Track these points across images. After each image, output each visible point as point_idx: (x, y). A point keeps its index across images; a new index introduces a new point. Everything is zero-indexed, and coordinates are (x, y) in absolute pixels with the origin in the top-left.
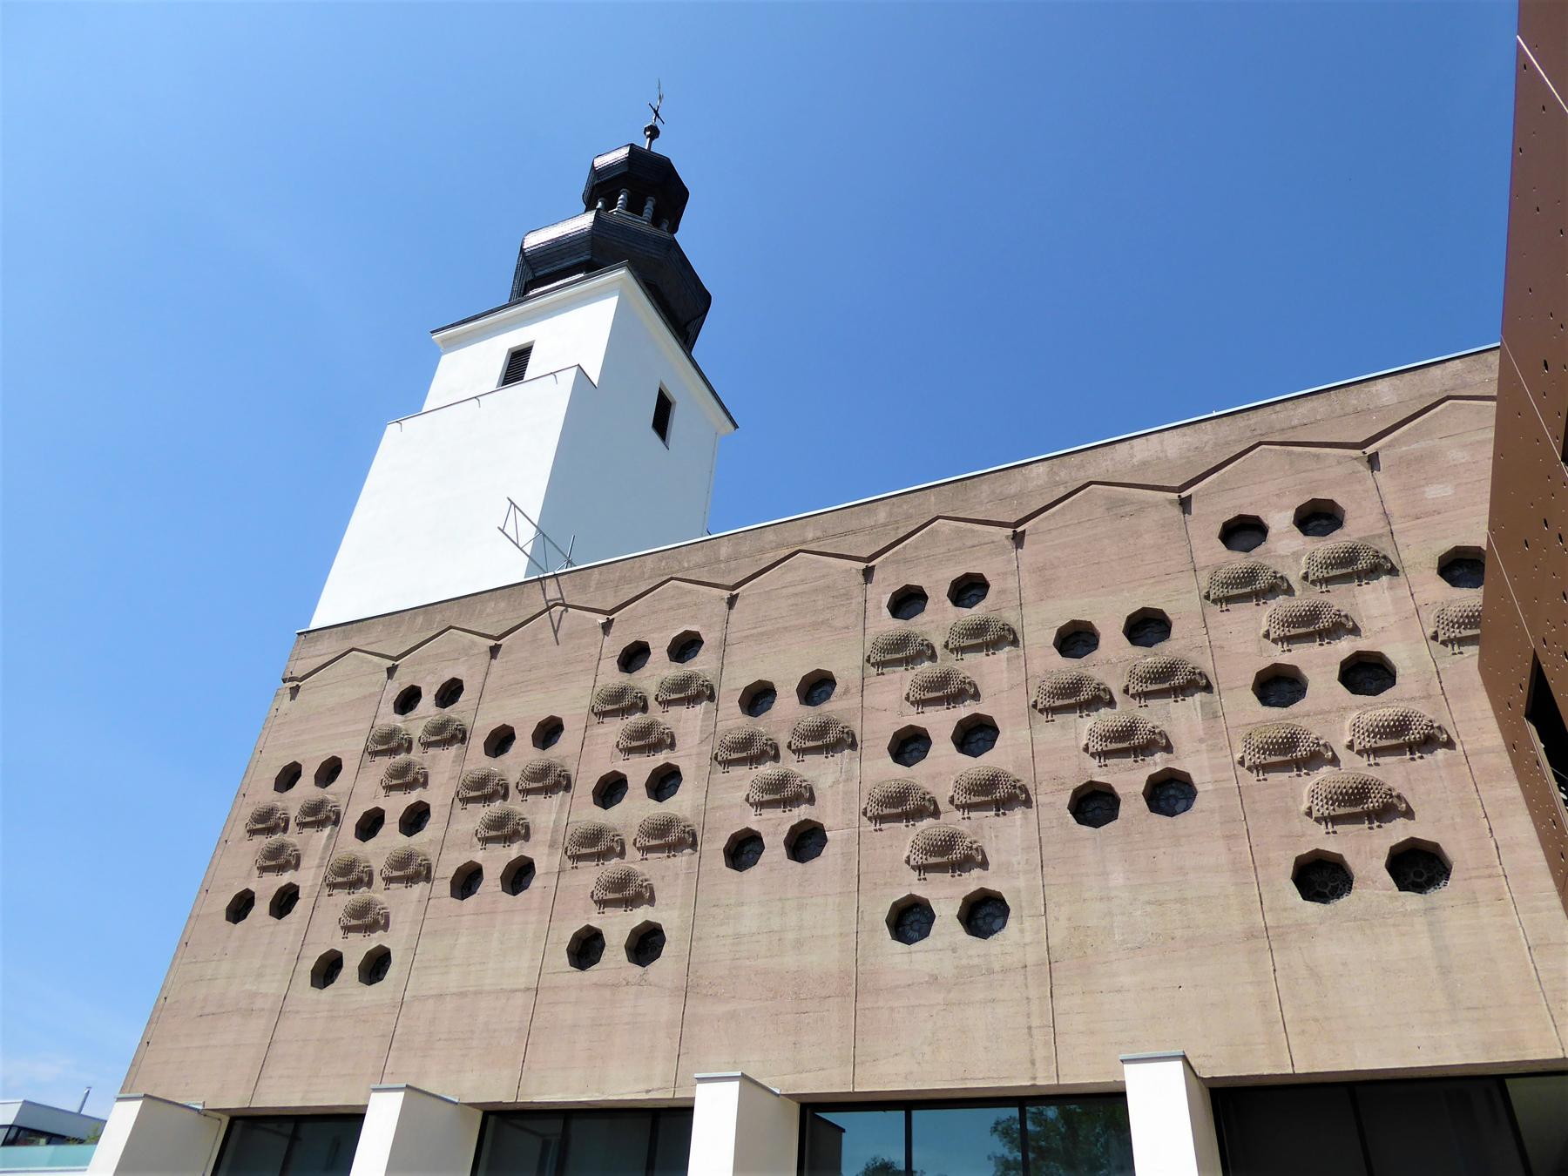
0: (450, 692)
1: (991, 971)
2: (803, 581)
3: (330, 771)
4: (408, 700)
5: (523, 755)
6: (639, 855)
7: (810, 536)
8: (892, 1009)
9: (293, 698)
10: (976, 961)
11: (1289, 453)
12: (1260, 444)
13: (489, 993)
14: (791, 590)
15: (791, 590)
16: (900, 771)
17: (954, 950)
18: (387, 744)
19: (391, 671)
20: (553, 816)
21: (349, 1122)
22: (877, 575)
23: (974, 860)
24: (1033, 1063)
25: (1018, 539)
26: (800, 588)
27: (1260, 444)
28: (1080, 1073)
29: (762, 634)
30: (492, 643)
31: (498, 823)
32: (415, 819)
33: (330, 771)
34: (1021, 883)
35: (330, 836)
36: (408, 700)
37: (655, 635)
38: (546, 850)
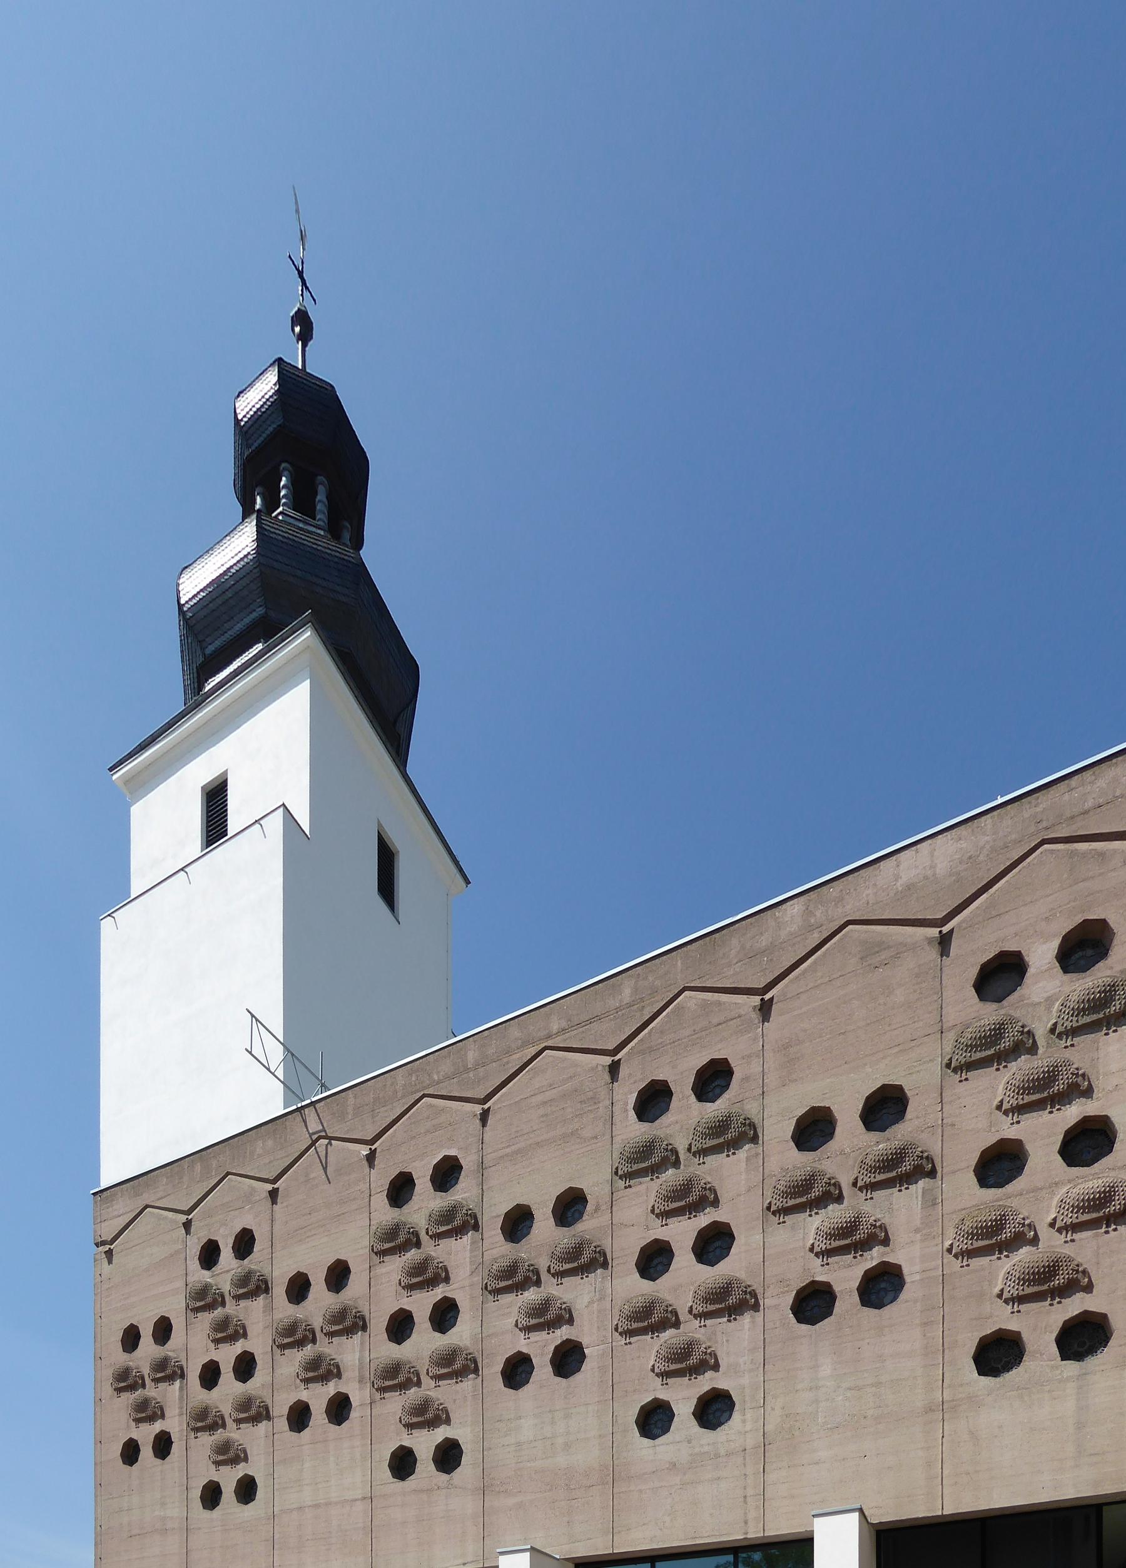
1: (717, 1456)
2: (551, 1086)
6: (432, 1383)
7: (555, 1027)
8: (641, 1491)
10: (706, 1449)
11: (1073, 854)
13: (336, 1503)
14: (540, 1098)
15: (540, 1098)
17: (689, 1442)
20: (357, 1355)
22: (623, 1071)
23: (440, 1418)
24: (746, 1522)
25: (187, 1225)
26: (549, 1095)
28: (780, 1527)
29: (517, 1152)
32: (245, 1367)
34: (746, 1380)
37: (416, 1164)
38: (357, 1385)
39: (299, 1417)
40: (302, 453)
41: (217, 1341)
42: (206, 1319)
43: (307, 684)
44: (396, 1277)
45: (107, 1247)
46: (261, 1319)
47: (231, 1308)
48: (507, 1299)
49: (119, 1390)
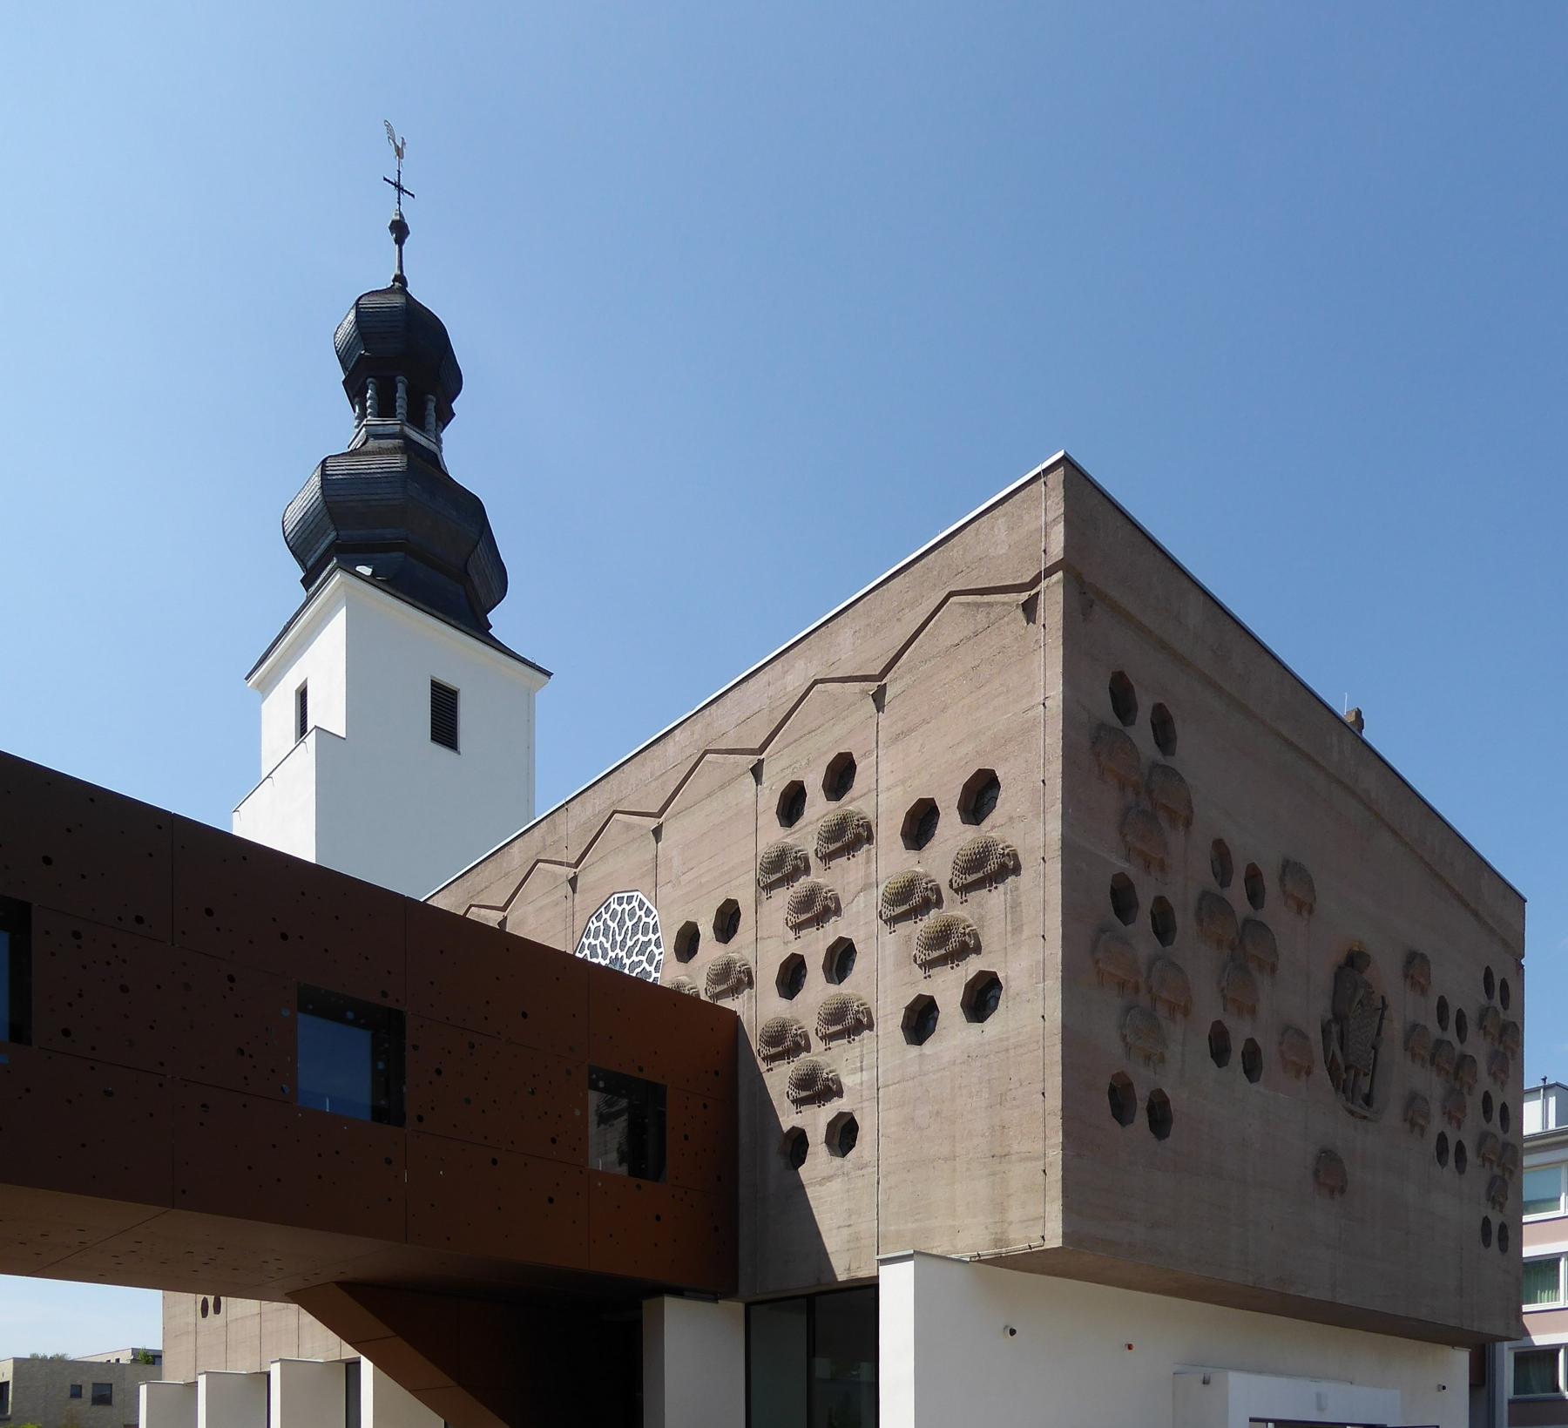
0: (841, 775)
3: (728, 921)
4: (792, 804)
5: (953, 836)
6: (822, 1046)
9: (880, 707)
12: (816, 682)
16: (834, 989)
18: (780, 869)
19: (757, 771)
21: (194, 1385)
22: (766, 771)
23: (831, 1090)
25: (879, 698)
27: (816, 682)
28: (864, 1273)
30: (1024, 596)
31: (941, 937)
32: (841, 959)
33: (728, 921)
35: (750, 998)
36: (792, 804)
39: (920, 1020)
40: (400, 358)
41: (798, 927)
42: (784, 897)
43: (344, 610)
44: (783, 914)
45: (1024, 596)
46: (861, 886)
47: (819, 876)
48: (905, 928)
49: (893, 921)
